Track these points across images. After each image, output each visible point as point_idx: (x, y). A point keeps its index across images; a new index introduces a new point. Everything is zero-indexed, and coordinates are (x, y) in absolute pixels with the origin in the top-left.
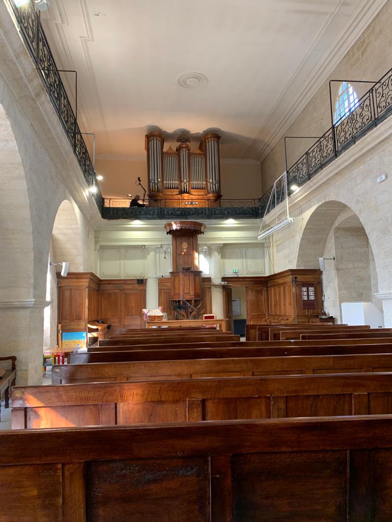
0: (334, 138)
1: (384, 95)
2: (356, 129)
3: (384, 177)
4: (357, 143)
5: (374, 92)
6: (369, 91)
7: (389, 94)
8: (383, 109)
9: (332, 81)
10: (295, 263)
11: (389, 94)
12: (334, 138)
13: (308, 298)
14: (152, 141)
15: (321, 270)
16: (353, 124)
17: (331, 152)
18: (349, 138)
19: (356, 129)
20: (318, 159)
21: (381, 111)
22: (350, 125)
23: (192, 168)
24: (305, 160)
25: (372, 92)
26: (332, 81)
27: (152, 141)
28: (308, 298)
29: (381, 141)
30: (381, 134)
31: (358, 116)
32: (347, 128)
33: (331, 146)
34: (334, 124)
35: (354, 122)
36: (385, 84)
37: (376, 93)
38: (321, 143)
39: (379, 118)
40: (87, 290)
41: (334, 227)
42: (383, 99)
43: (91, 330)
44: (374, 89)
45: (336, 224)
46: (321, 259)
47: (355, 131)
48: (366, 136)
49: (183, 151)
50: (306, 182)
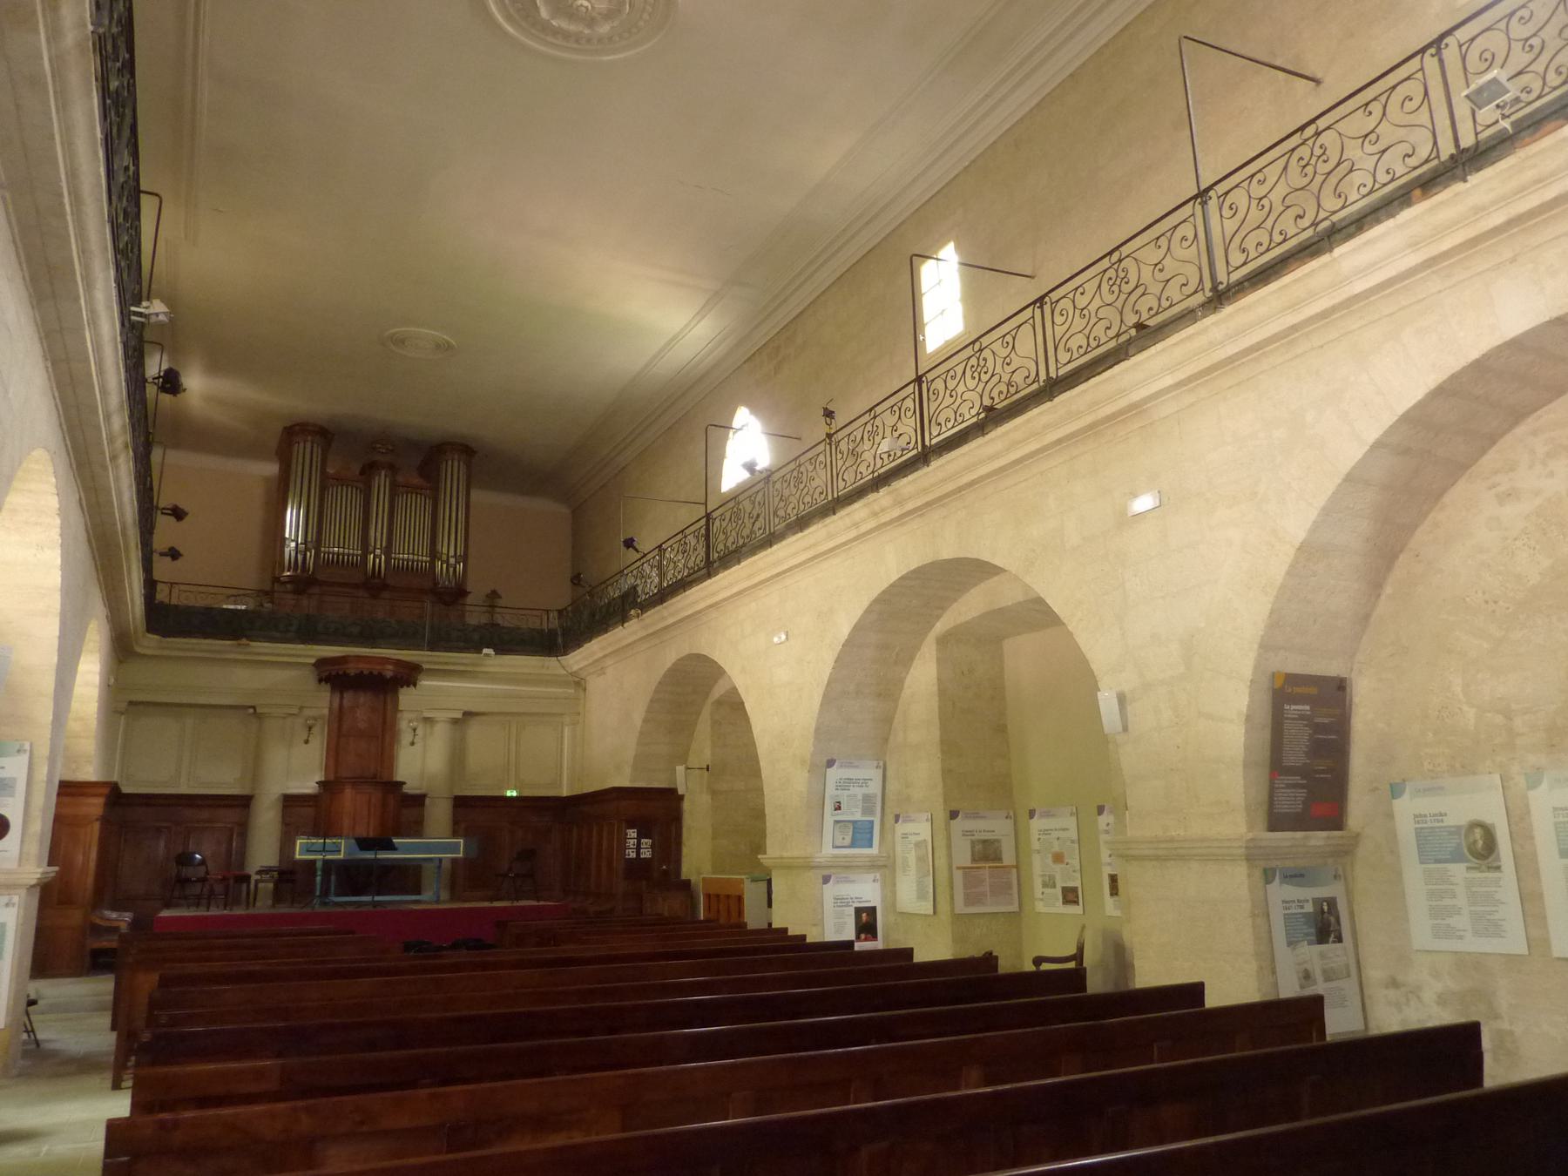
0: (707, 536)
1: (783, 498)
2: (743, 537)
3: (783, 637)
4: (742, 564)
5: (1047, 308)
6: (1034, 303)
7: (1287, 202)
8: (1076, 355)
9: (711, 425)
10: (628, 770)
11: (1287, 202)
12: (707, 536)
13: (638, 853)
14: (302, 445)
15: (680, 793)
16: (1123, 297)
17: (703, 563)
18: (967, 417)
19: (743, 537)
20: (792, 505)
21: (939, 435)
22: (734, 525)
23: (398, 519)
24: (760, 494)
25: (1041, 307)
26: (711, 425)
27: (302, 445)
28: (638, 853)
29: (1026, 455)
30: (968, 468)
31: (747, 515)
32: (1092, 307)
33: (702, 551)
34: (920, 374)
35: (801, 486)
36: (952, 373)
37: (928, 391)
38: (800, 466)
39: (777, 533)
40: (97, 826)
41: (940, 627)
42: (782, 504)
43: (140, 315)
44: (1047, 299)
45: (940, 627)
46: (680, 769)
47: (802, 507)
48: (756, 557)
49: (380, 476)
50: (655, 607)
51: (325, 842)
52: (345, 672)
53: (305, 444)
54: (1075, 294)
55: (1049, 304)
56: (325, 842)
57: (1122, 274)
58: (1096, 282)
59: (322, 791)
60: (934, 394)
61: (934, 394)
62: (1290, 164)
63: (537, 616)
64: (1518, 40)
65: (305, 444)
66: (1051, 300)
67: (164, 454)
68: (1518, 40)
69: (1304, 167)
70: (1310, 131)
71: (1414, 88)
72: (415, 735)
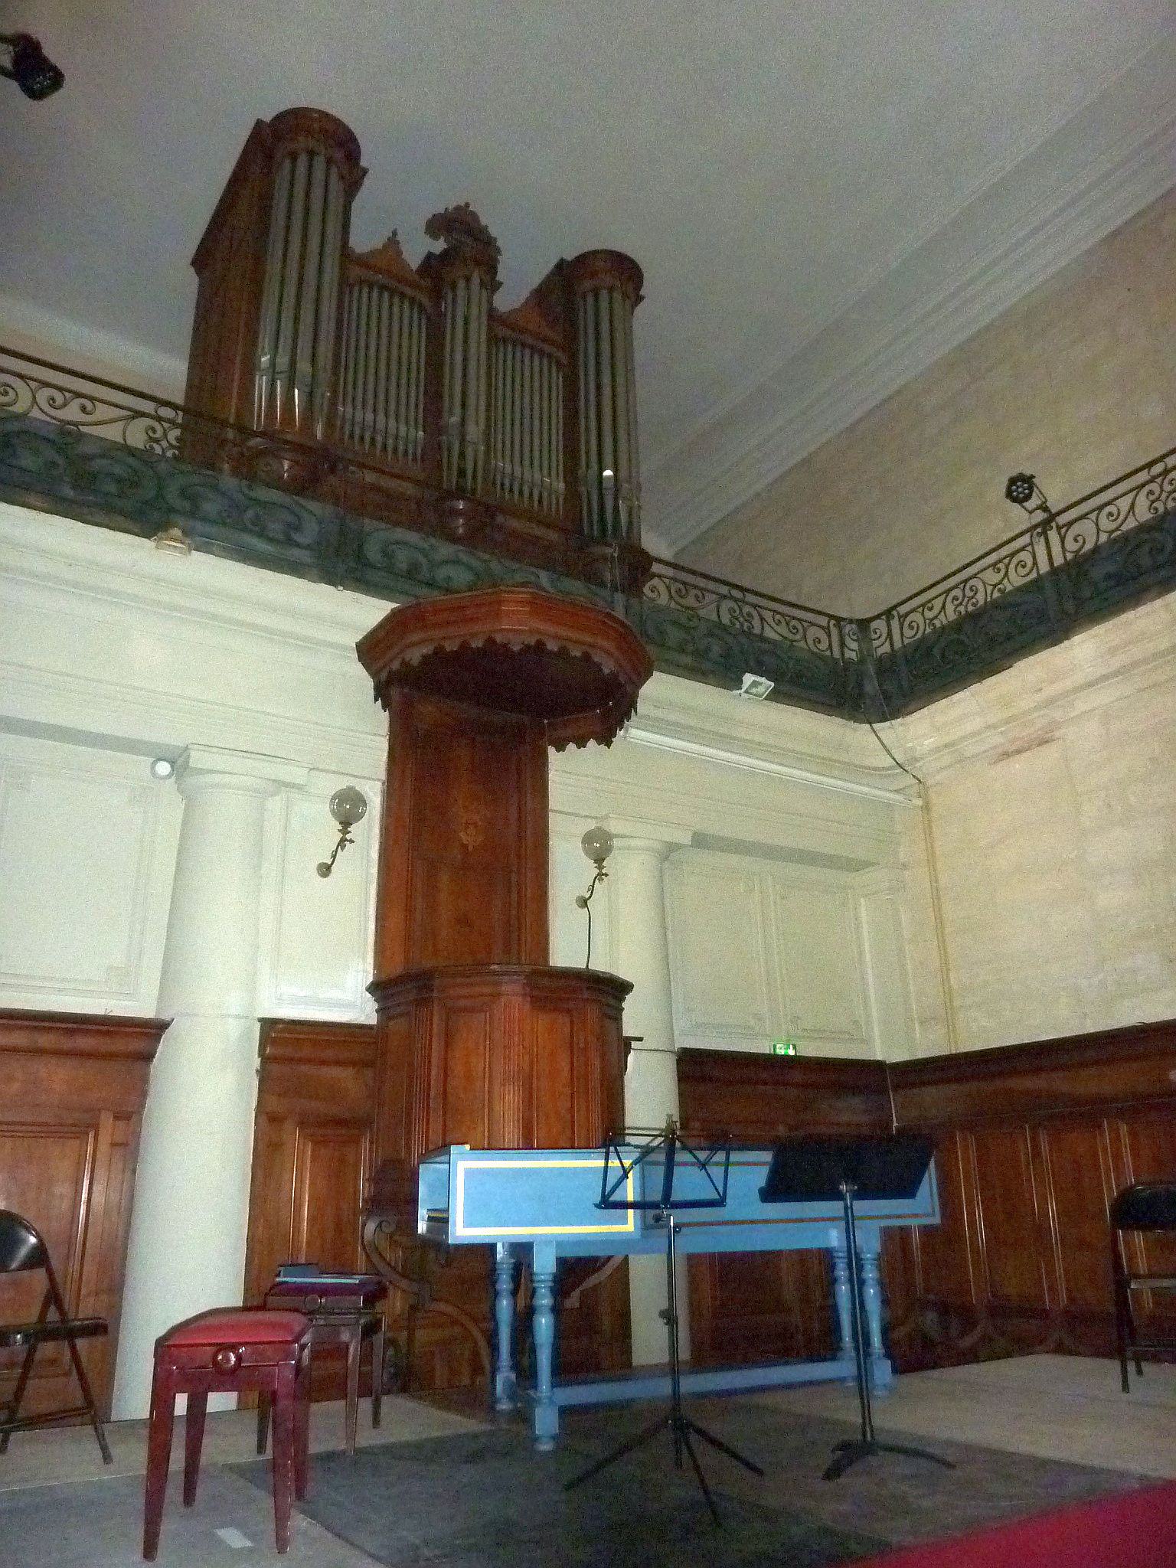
25: (1044, 533)
44: (894, 613)
51: (606, 1167)
52: (491, 641)
53: (311, 160)
54: (1098, 515)
55: (896, 618)
56: (606, 1167)
57: (969, 594)
58: (941, 599)
59: (638, 1236)
60: (912, 628)
61: (912, 628)
62: (1137, 501)
63: (822, 627)
64: (1106, 532)
65: (311, 160)
66: (898, 614)
67: (588, 966)
68: (1106, 532)
69: (1153, 502)
70: (1158, 468)
71: (1026, 556)
72: (342, 843)
